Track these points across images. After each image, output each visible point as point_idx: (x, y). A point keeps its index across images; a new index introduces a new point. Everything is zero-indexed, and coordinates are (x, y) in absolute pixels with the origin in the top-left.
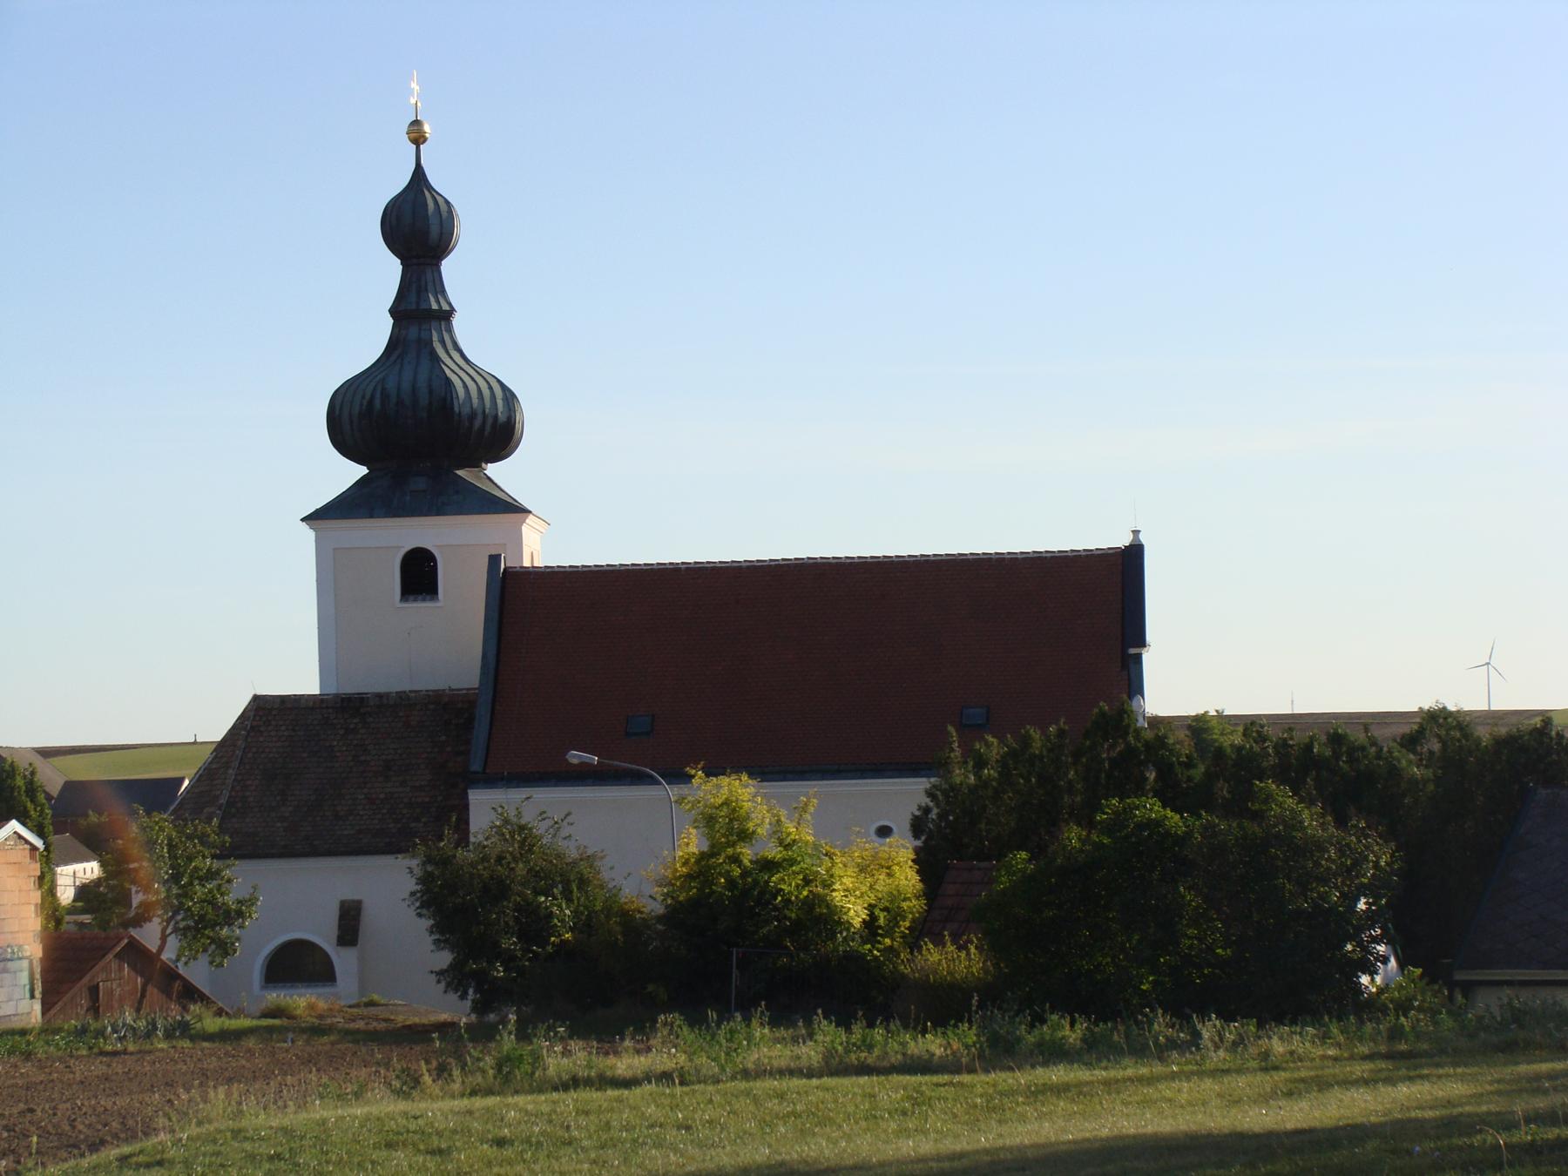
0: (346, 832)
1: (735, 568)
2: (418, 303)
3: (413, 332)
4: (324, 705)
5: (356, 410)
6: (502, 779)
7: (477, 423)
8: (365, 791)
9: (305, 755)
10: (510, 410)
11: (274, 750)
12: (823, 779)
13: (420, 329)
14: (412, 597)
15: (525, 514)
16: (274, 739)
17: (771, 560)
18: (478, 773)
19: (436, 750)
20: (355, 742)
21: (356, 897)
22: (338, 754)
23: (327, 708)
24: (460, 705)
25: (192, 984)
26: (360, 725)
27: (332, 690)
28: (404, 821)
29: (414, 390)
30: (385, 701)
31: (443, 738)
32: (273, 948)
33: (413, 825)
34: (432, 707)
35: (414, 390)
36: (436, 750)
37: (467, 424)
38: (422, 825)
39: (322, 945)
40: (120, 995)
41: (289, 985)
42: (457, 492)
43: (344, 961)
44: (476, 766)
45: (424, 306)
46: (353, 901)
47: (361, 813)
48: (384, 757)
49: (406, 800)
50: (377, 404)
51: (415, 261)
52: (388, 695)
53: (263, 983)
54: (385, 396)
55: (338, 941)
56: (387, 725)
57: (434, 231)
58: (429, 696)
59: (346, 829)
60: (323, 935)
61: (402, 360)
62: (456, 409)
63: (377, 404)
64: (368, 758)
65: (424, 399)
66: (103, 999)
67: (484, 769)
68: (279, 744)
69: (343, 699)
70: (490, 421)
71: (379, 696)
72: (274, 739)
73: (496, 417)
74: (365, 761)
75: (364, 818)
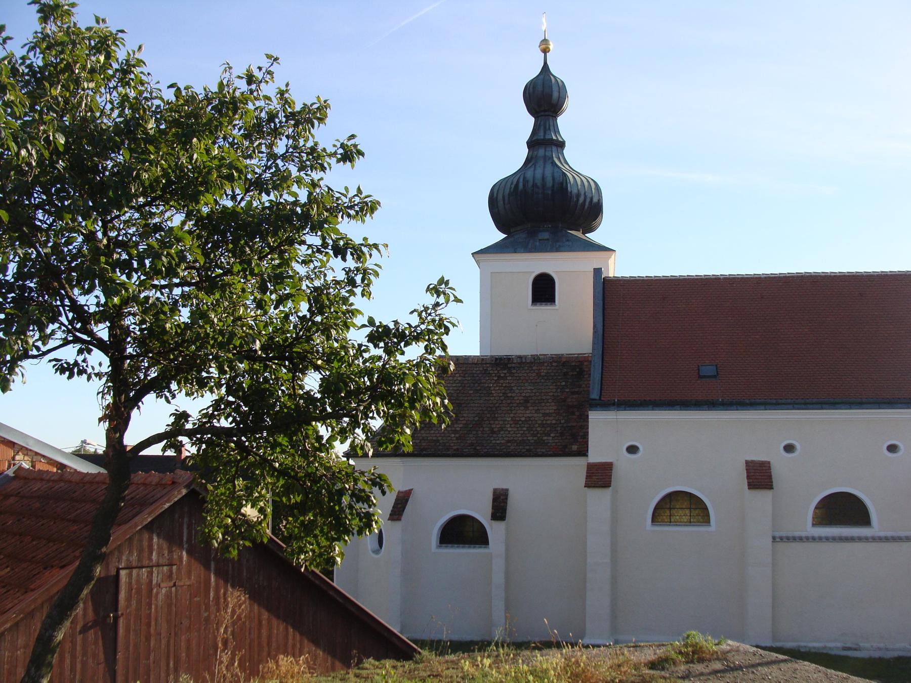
0: (498, 442)
1: (756, 278)
2: (544, 136)
3: (541, 152)
4: (484, 362)
5: (507, 191)
6: (614, 404)
7: (581, 199)
8: (512, 415)
9: (472, 392)
10: (599, 196)
11: (451, 388)
12: (851, 409)
13: (545, 151)
14: (538, 304)
15: (611, 252)
16: (451, 382)
17: (780, 274)
18: (596, 400)
19: (559, 390)
20: (504, 385)
21: (505, 487)
22: (493, 392)
23: (486, 364)
24: (573, 364)
25: (588, 251)
26: (508, 375)
27: (488, 353)
28: (539, 435)
29: (543, 178)
30: (524, 361)
31: (564, 383)
32: (448, 518)
33: (545, 438)
34: (554, 364)
35: (543, 178)
36: (559, 390)
37: (575, 199)
38: (551, 438)
39: (479, 519)
40: (168, 595)
41: (456, 545)
42: (568, 240)
43: (495, 530)
44: (594, 395)
45: (548, 137)
46: (503, 489)
47: (509, 429)
48: (524, 394)
49: (540, 422)
50: (521, 185)
51: (542, 113)
52: (526, 357)
53: (439, 544)
54: (526, 181)
55: (492, 516)
56: (525, 375)
57: (555, 95)
58: (553, 358)
59: (498, 440)
60: (482, 513)
61: (535, 166)
62: (569, 189)
63: (521, 185)
64: (513, 395)
65: (549, 183)
66: (128, 599)
67: (600, 397)
68: (454, 385)
69: (496, 359)
70: (588, 200)
71: (520, 357)
72: (451, 382)
73: (592, 199)
74: (511, 396)
75: (511, 433)
